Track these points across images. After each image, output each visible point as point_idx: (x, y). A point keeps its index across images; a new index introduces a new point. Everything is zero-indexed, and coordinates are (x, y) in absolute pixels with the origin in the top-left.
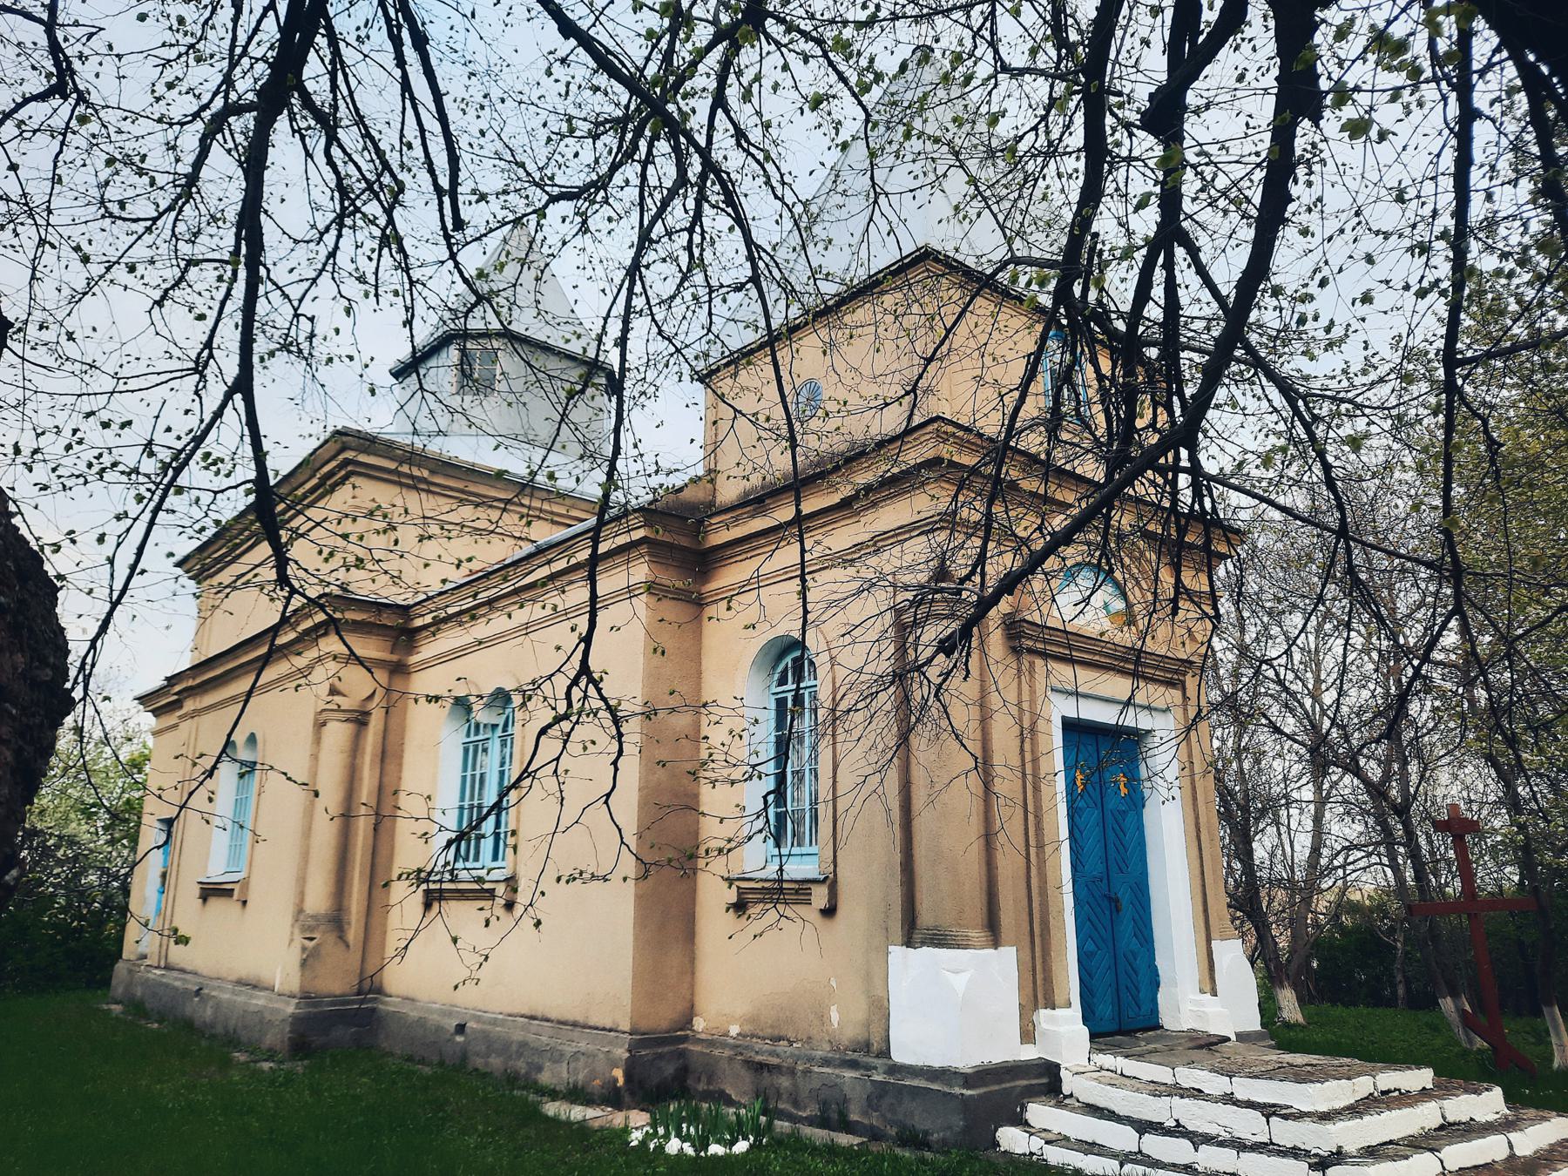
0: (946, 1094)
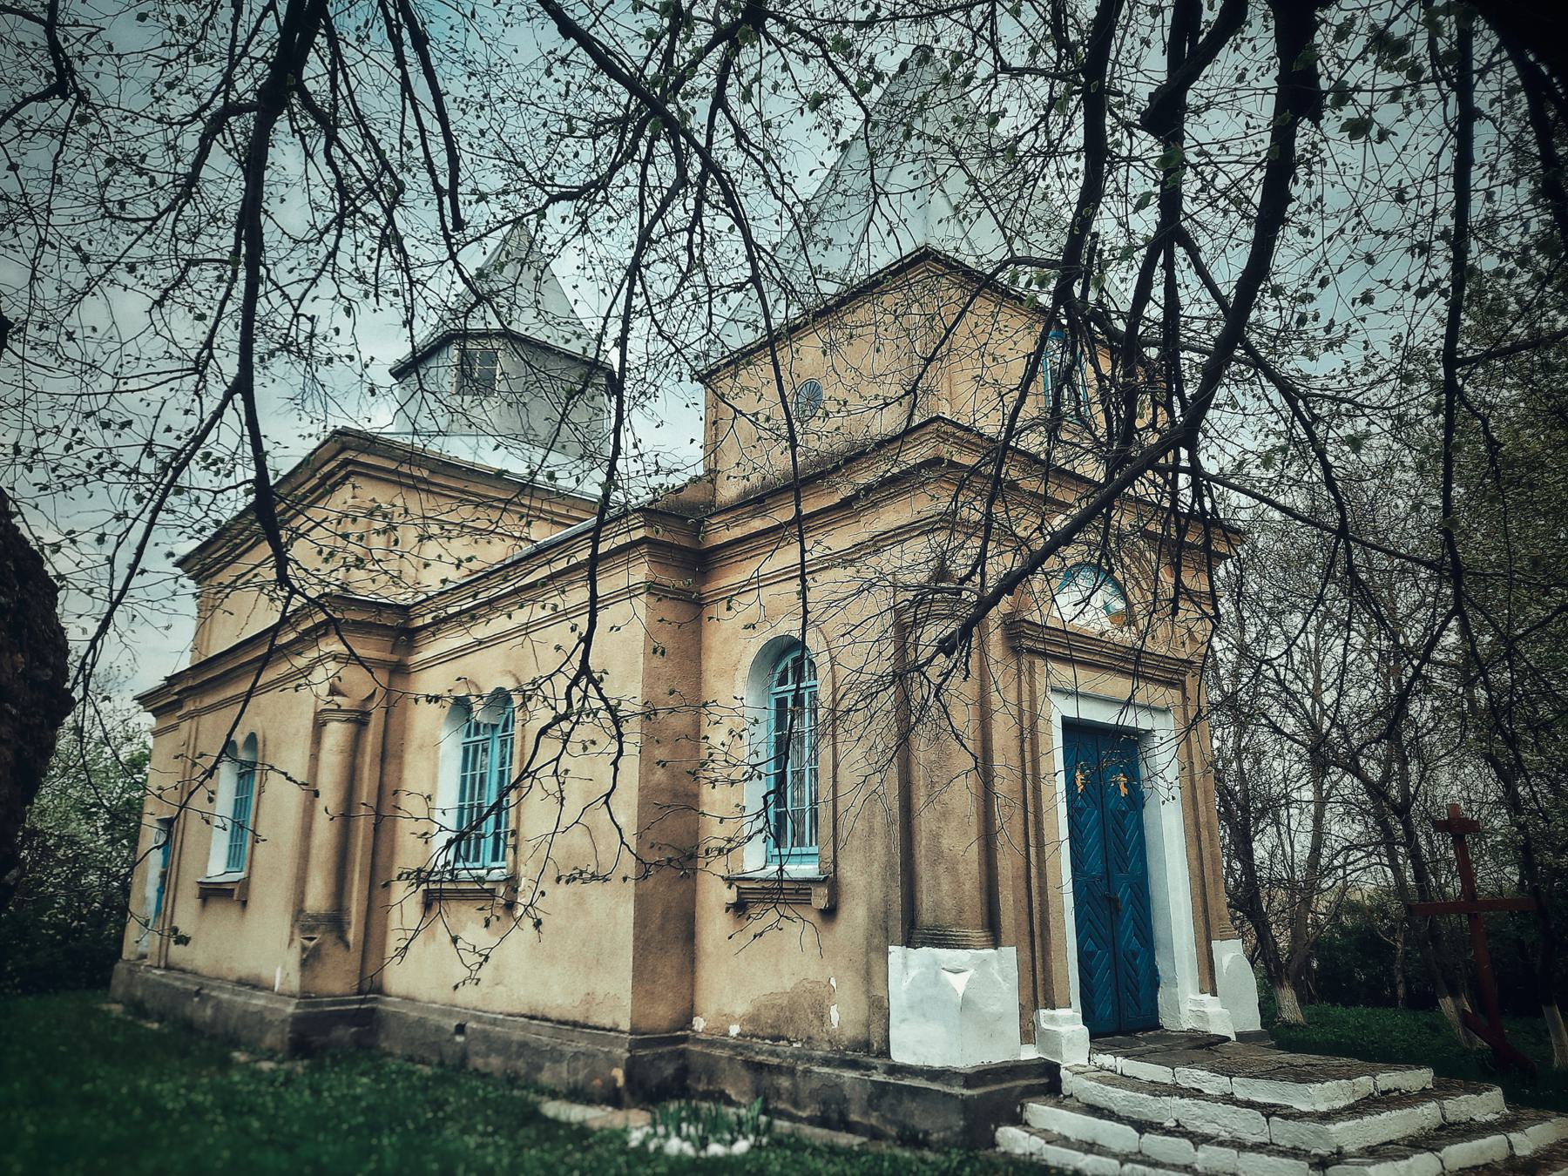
0: (946, 1095)
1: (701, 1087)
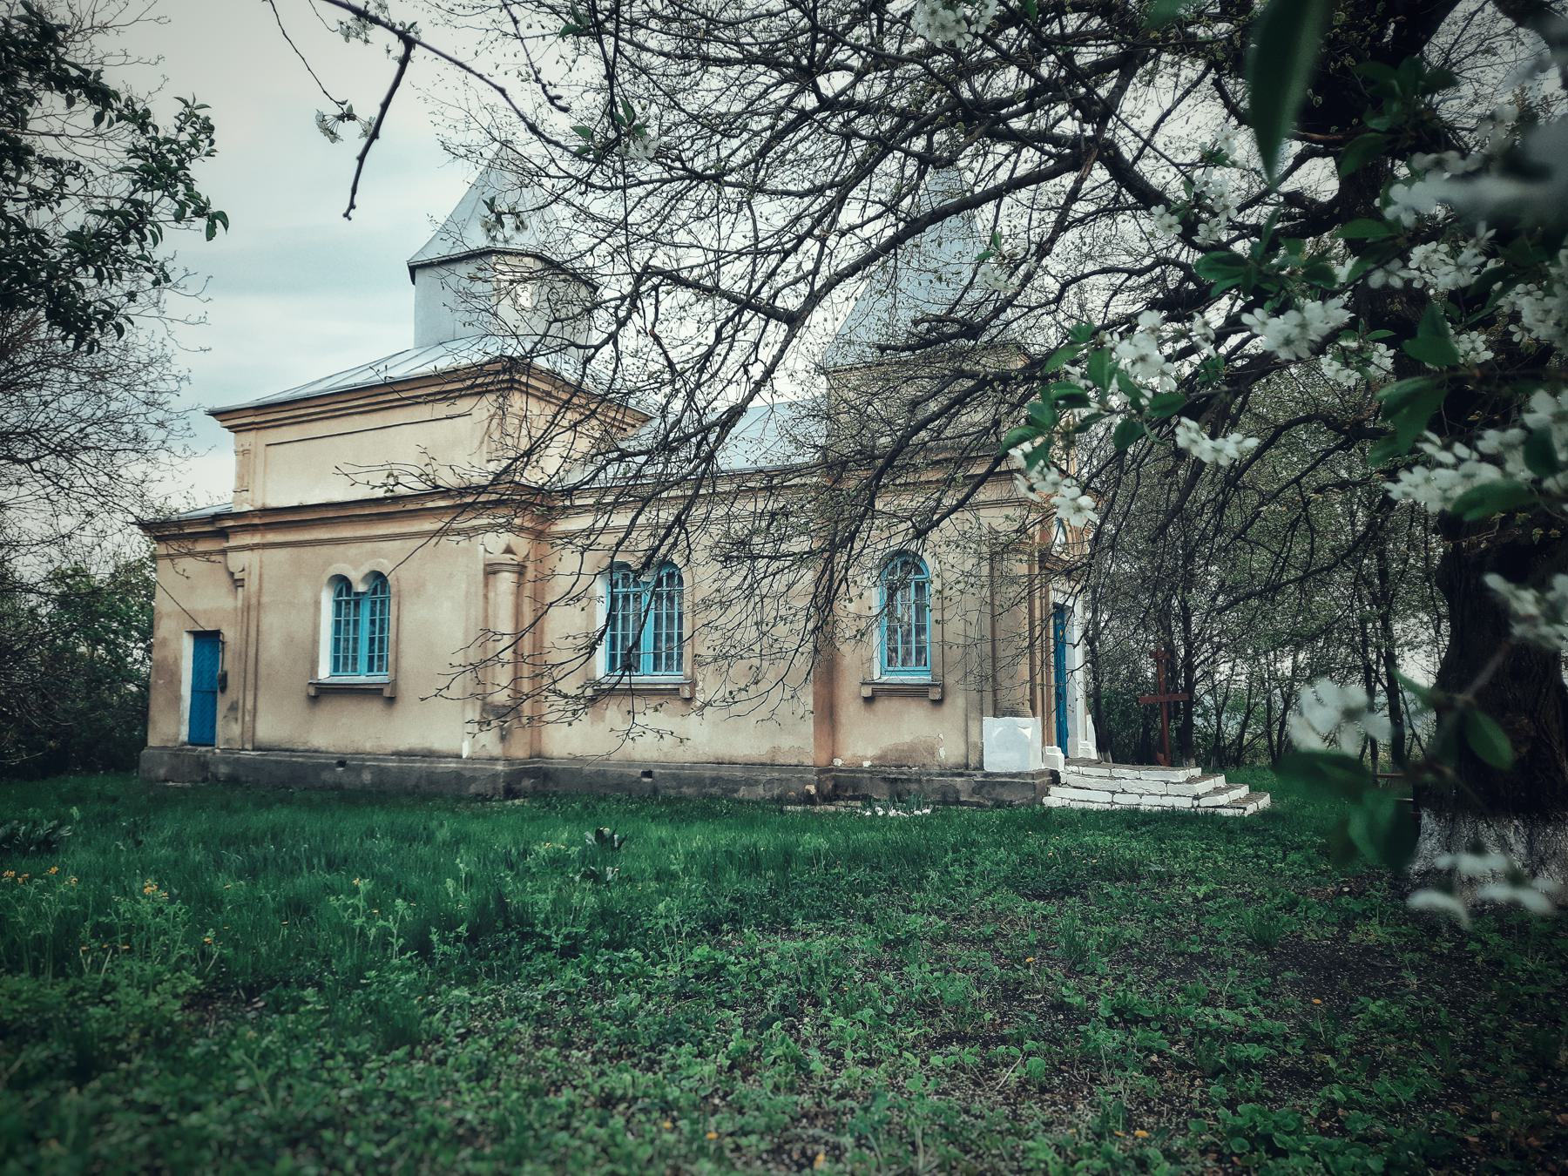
1: (850, 793)
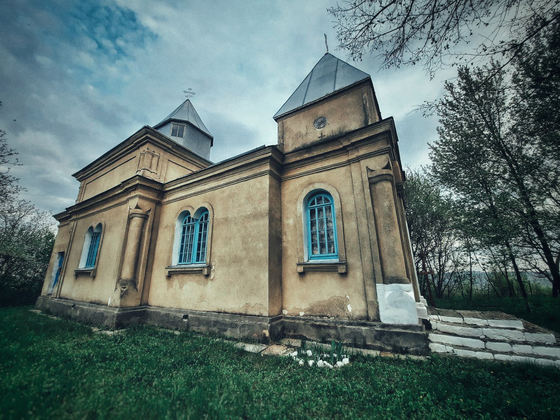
0: (414, 334)
1: (291, 333)
